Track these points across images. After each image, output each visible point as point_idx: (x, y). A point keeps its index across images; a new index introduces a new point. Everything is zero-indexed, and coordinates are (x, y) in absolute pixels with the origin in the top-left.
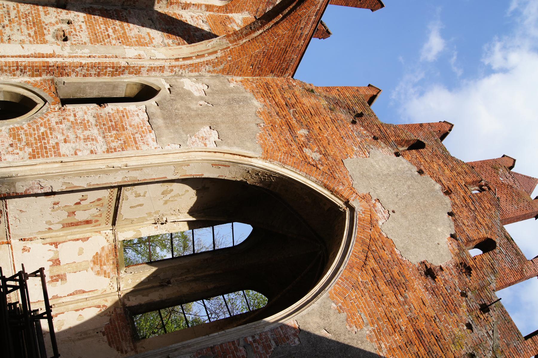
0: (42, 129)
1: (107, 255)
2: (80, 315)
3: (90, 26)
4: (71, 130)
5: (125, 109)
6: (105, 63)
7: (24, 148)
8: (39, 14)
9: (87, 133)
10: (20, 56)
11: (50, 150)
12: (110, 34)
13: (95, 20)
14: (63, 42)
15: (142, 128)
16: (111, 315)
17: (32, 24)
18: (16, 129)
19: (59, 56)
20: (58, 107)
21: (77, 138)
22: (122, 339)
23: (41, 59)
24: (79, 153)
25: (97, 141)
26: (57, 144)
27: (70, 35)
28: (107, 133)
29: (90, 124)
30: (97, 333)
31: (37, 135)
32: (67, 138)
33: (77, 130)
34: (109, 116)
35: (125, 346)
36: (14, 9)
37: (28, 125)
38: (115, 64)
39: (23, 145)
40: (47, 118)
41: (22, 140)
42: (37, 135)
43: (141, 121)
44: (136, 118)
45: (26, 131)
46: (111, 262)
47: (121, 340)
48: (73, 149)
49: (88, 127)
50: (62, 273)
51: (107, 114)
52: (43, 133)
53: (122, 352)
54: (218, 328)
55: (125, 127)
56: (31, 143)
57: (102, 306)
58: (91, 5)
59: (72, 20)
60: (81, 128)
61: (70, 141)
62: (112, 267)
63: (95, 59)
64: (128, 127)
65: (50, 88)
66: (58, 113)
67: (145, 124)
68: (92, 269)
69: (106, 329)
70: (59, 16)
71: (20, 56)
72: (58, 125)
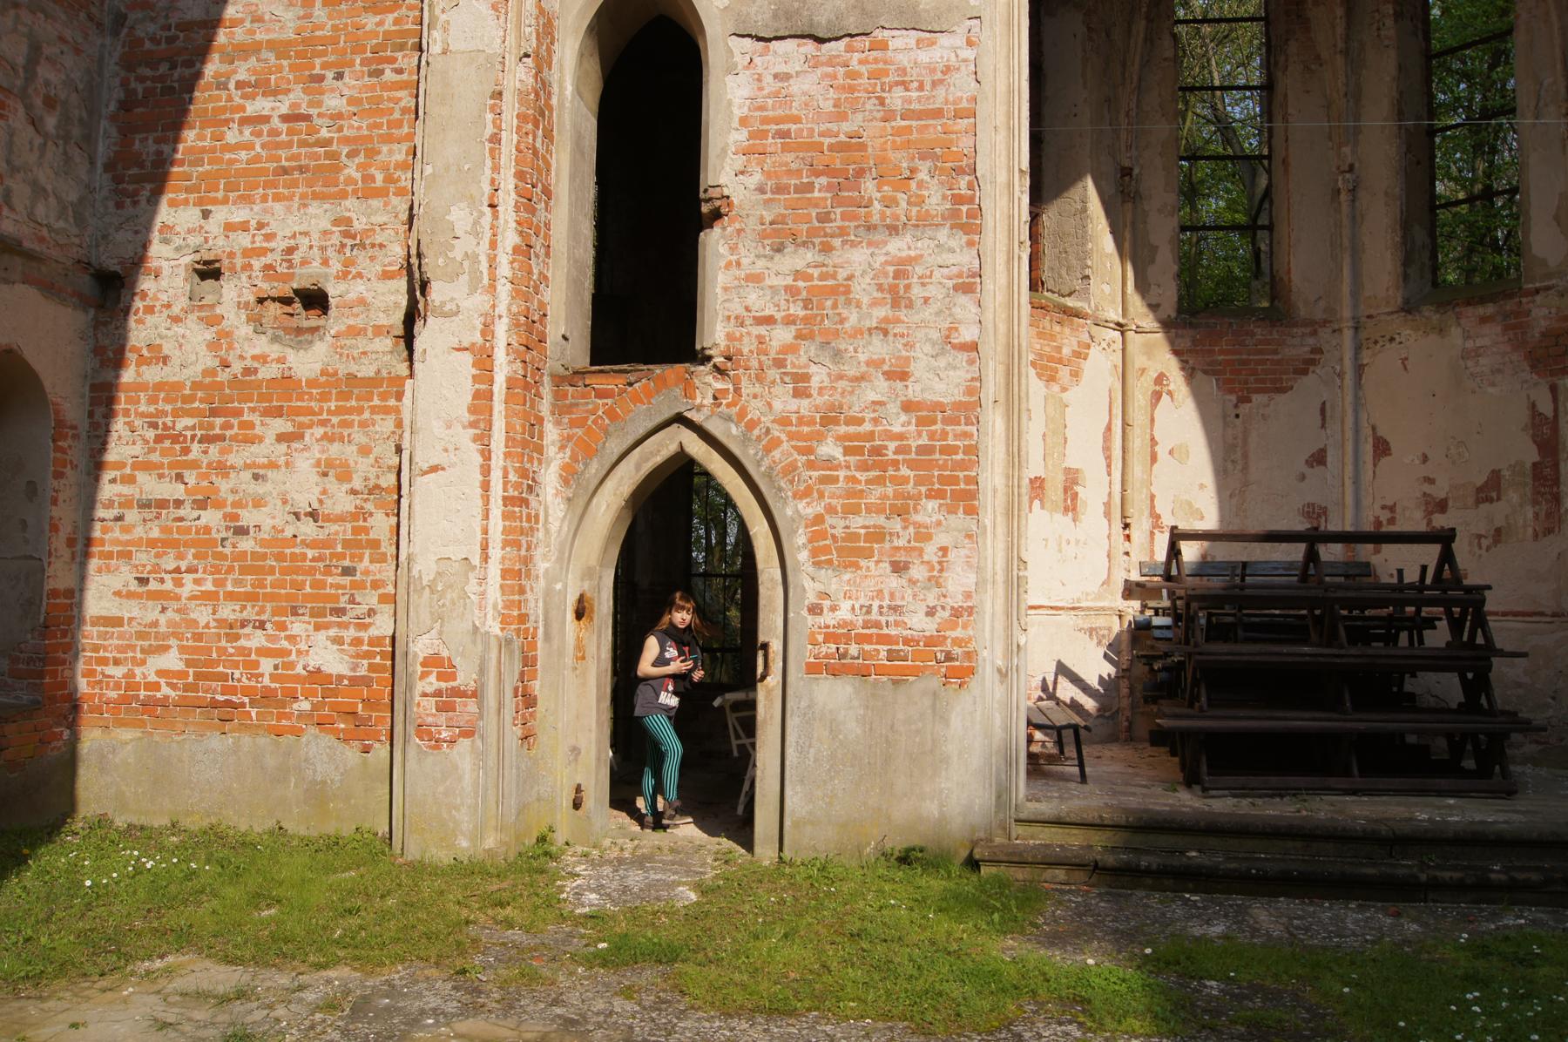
0: (830, 449)
1: (1040, 335)
2: (1171, 452)
3: (229, 188)
4: (842, 347)
5: (744, 121)
6: (519, 150)
7: (917, 525)
8: (159, 386)
9: (863, 289)
10: (486, 486)
11: (937, 437)
12: (284, 110)
13: (200, 162)
14: (333, 312)
15: (853, 75)
16: (1193, 369)
17: (219, 421)
18: (821, 543)
19: (487, 330)
20: (709, 379)
21: (886, 333)
22: (1275, 352)
23: (499, 406)
24: (967, 334)
25: (910, 261)
26: (908, 407)
27: (291, 277)
28: (868, 215)
29: (816, 272)
30: (1237, 416)
31: (858, 475)
32: (886, 368)
33: (847, 325)
34: (779, 189)
35: (1296, 347)
36: (130, 480)
37: (801, 498)
38: (523, 109)
39: (905, 528)
40: (769, 425)
41: (875, 526)
42: (858, 475)
43: (818, 72)
44: (795, 87)
45: (831, 510)
46: (1057, 328)
47: (1276, 357)
48: (942, 353)
49: (830, 282)
50: (1061, 477)
51: (769, 196)
52: (847, 451)
53: (1313, 362)
54: (1313, 67)
55: (842, 138)
56: (895, 497)
57: (1158, 388)
58: (99, 164)
59: (197, 257)
60: (835, 306)
61: (899, 358)
62: (1067, 330)
63: (502, 186)
64: (846, 127)
65: (601, 394)
66: (744, 383)
67: (838, 56)
68: (1064, 389)
69: (1231, 391)
70: (168, 306)
71: (486, 486)
72: (814, 392)
